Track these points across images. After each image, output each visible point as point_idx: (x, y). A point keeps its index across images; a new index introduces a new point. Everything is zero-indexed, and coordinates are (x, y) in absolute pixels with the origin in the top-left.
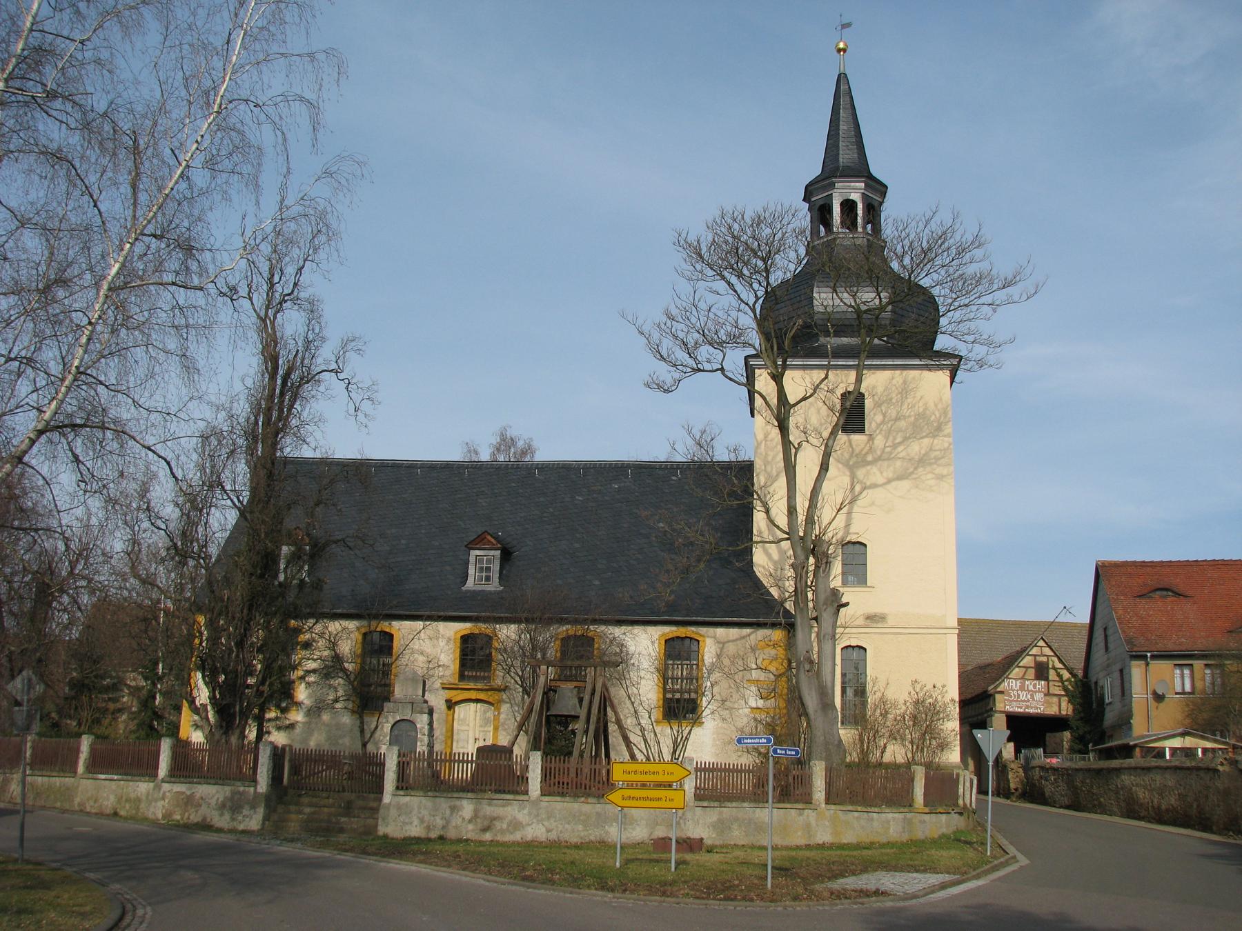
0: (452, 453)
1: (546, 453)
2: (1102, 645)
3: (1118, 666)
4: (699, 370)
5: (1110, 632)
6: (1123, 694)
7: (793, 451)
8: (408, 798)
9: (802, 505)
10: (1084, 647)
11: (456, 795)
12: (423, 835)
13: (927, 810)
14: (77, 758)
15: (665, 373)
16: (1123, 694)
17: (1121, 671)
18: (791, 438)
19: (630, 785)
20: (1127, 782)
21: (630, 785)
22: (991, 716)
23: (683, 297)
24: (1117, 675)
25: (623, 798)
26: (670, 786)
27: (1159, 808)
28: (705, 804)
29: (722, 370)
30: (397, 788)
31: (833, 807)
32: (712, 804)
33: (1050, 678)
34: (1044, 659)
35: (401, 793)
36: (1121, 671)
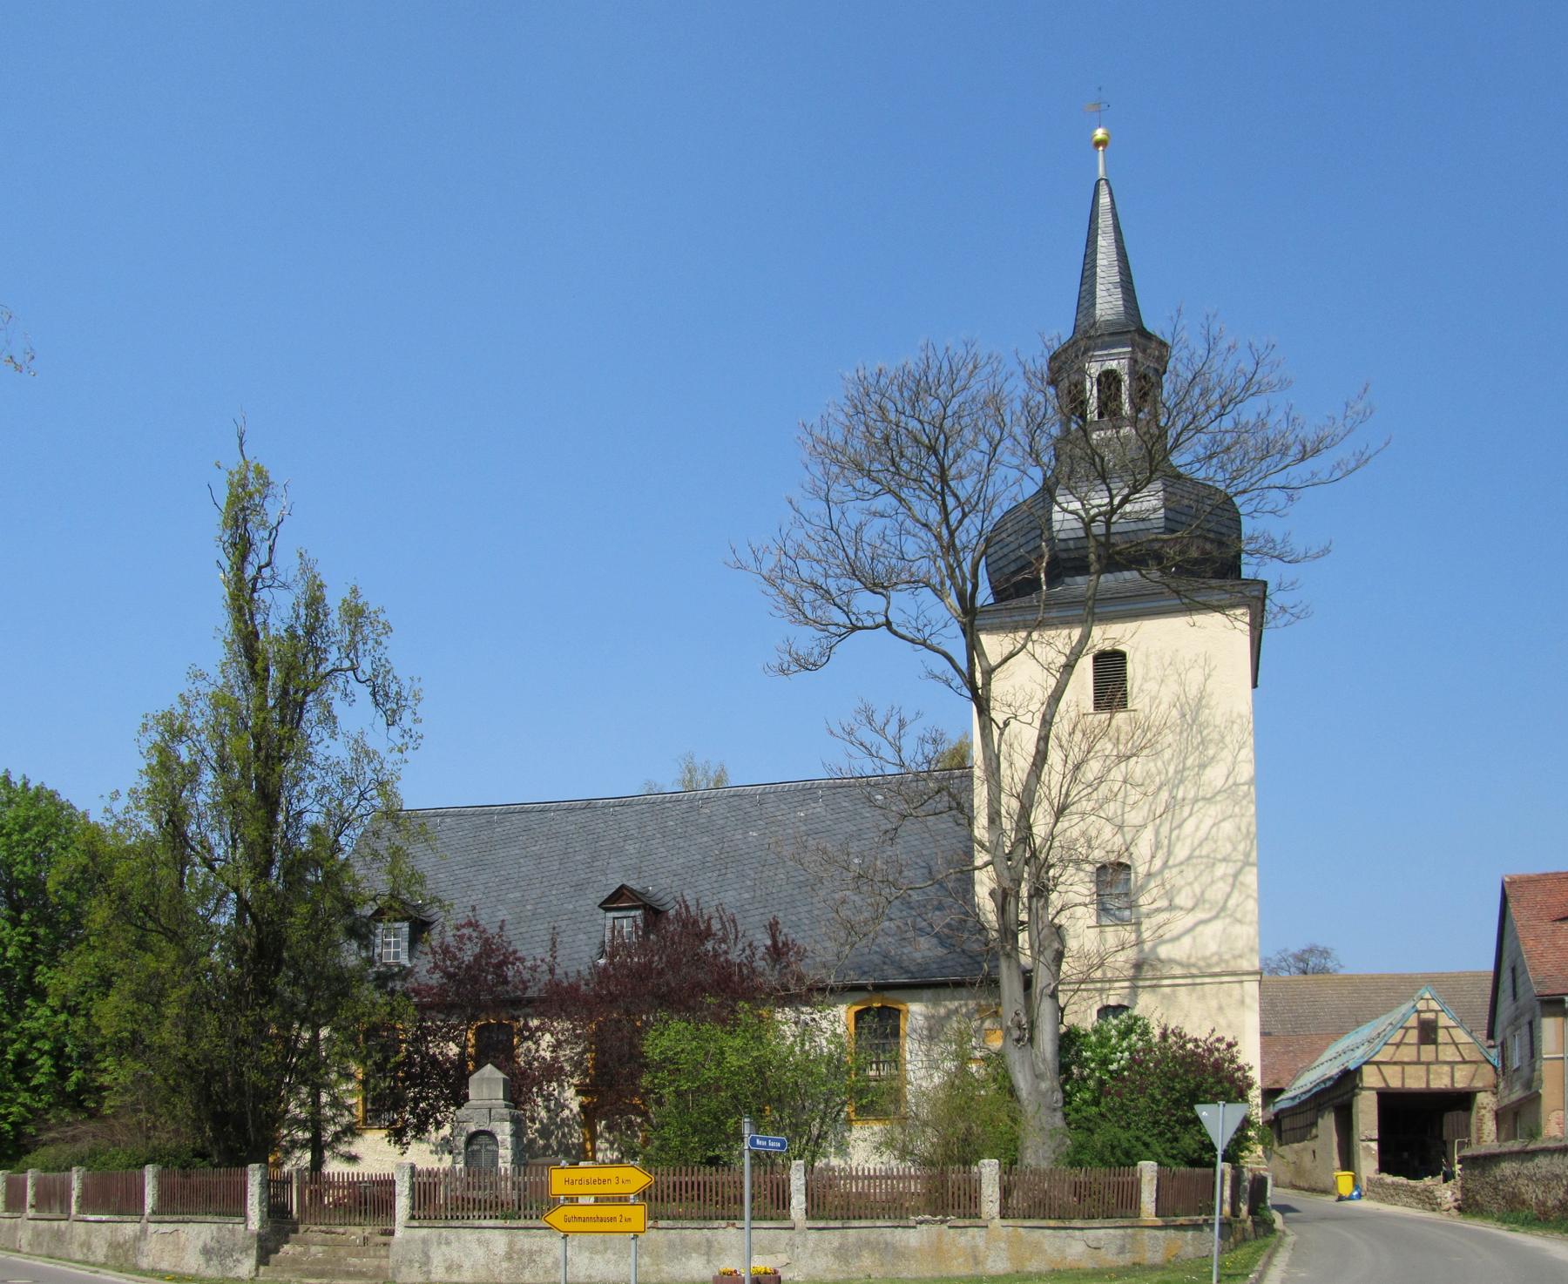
0: (630, 787)
1: (739, 777)
2: (1509, 992)
3: (1526, 1018)
4: (854, 628)
5: (1519, 971)
6: (1532, 1056)
7: (996, 732)
8: (424, 1232)
9: (1010, 804)
10: (1489, 991)
11: (1077, 1223)
12: (1088, 1264)
13: (1159, 1222)
14: (70, 1196)
15: (807, 639)
16: (1532, 1056)
17: (1530, 1023)
18: (993, 714)
19: (622, 1199)
20: (1508, 1172)
21: (622, 1199)
22: (1355, 1095)
23: (816, 521)
24: (1525, 1029)
25: (567, 1220)
26: (626, 1199)
27: (1544, 1204)
28: (821, 1224)
29: (888, 624)
30: (412, 1217)
31: (1010, 1222)
32: (832, 1224)
33: (1440, 1040)
34: (1431, 1016)
35: (415, 1223)
36: (1530, 1023)
